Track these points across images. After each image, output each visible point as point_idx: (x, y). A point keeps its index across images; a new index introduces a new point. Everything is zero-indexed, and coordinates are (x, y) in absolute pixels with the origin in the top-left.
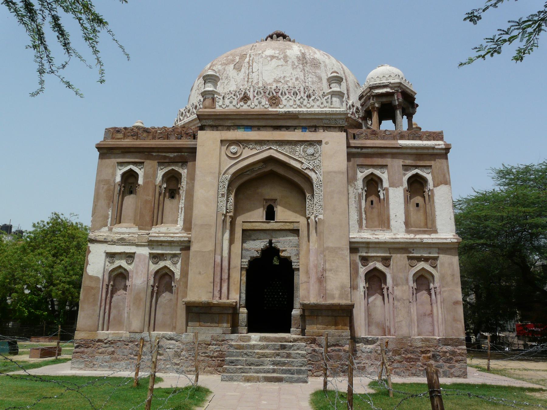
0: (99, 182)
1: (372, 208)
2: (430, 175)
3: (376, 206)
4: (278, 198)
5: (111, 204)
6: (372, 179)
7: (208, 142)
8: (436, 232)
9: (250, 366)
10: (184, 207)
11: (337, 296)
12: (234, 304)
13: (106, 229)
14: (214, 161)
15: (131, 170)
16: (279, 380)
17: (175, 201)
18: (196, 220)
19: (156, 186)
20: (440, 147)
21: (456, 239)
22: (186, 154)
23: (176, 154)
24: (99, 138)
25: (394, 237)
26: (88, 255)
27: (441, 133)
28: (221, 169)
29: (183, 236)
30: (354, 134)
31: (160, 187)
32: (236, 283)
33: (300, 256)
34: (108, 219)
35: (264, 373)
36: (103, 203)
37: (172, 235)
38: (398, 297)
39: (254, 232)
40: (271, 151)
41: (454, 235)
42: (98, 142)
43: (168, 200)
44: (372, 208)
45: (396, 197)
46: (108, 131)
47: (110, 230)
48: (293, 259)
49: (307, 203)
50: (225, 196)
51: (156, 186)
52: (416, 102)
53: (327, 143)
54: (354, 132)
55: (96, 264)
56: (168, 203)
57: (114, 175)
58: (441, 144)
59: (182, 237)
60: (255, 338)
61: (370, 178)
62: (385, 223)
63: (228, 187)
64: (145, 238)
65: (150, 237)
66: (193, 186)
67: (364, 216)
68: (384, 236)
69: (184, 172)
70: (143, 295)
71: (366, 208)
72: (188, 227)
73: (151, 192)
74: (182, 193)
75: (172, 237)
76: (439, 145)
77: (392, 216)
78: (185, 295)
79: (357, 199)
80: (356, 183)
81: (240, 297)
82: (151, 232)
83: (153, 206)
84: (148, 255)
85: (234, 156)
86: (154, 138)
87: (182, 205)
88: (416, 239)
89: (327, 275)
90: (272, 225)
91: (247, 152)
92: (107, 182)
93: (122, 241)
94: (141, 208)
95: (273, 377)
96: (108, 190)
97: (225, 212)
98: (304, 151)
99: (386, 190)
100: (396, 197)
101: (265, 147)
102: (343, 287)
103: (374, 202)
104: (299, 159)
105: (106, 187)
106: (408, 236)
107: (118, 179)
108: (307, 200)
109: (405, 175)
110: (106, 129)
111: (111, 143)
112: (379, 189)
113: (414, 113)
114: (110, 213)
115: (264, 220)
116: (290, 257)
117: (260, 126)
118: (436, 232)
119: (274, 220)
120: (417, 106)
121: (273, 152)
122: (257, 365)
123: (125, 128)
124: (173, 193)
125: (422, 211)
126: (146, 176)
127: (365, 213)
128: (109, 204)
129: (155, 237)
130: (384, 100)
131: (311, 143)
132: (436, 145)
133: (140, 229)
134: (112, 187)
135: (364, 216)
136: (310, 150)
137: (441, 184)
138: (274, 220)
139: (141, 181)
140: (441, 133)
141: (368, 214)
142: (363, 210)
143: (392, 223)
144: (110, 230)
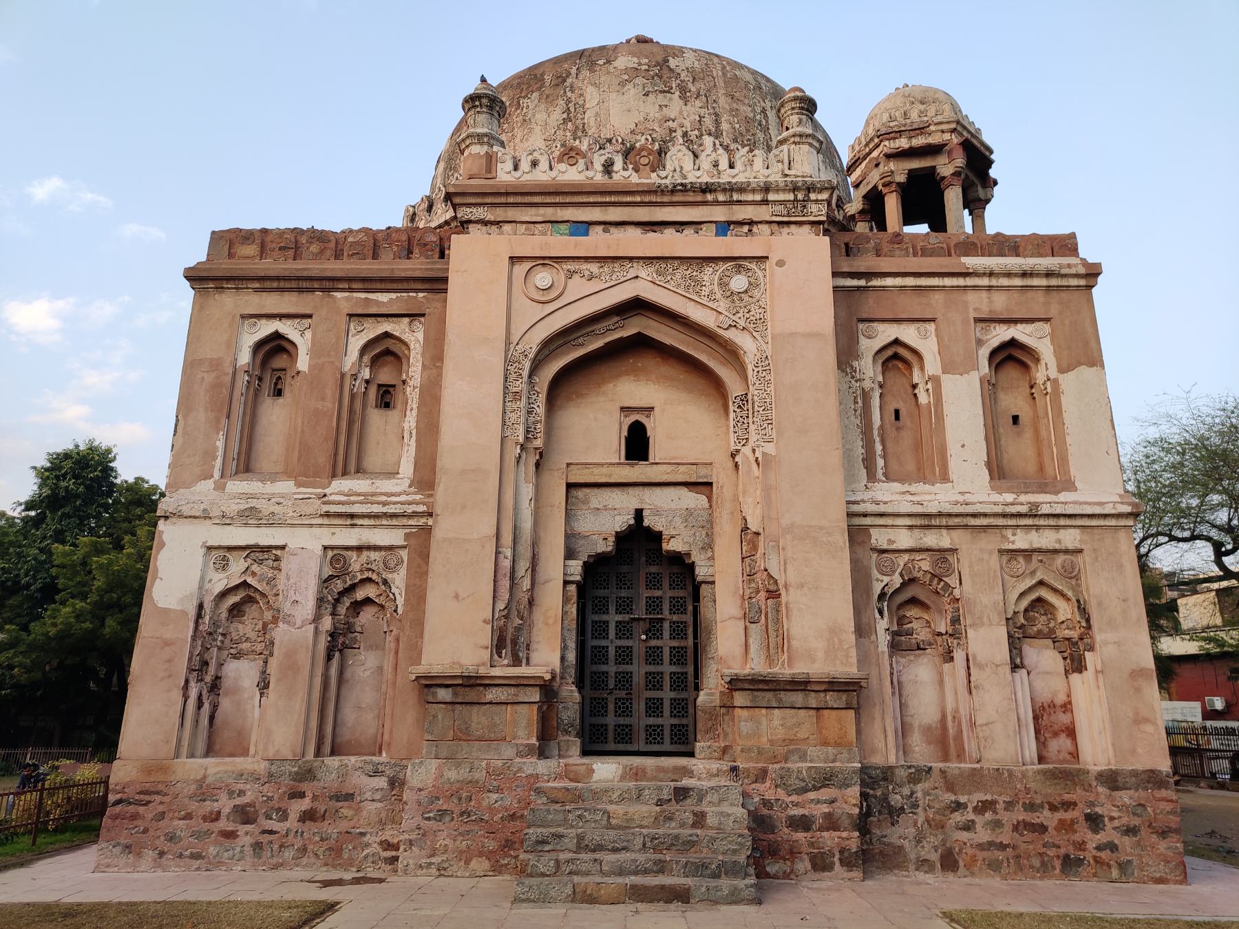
0: (191, 366)
1: (898, 429)
2: (1047, 341)
3: (909, 424)
4: (656, 404)
5: (224, 420)
6: (896, 356)
7: (476, 259)
8: (1070, 486)
9: (594, 851)
10: (417, 427)
11: (820, 655)
12: (548, 677)
13: (210, 484)
14: (495, 304)
15: (277, 336)
16: (680, 896)
17: (393, 415)
18: (449, 458)
19: (343, 376)
20: (1073, 271)
21: (1129, 504)
22: (421, 295)
23: (394, 296)
24: (198, 253)
25: (961, 498)
26: (158, 552)
27: (1073, 236)
28: (512, 332)
29: (414, 501)
30: (847, 245)
31: (355, 377)
32: (551, 622)
33: (716, 548)
34: (215, 458)
35: (636, 873)
36: (201, 416)
37: (384, 498)
38: (979, 658)
39: (596, 491)
40: (639, 282)
41: (1120, 496)
42: (192, 263)
43: (375, 411)
44: (898, 429)
45: (961, 404)
46: (217, 237)
47: (220, 487)
48: (698, 558)
49: (732, 415)
50: (524, 399)
51: (343, 376)
52: (993, 173)
53: (781, 263)
54: (847, 240)
55: (178, 574)
56: (376, 417)
57: (233, 345)
58: (1076, 265)
59: (410, 503)
60: (606, 770)
61: (890, 352)
62: (930, 464)
63: (530, 377)
64: (316, 506)
65: (325, 503)
66: (440, 375)
67: (879, 448)
68: (937, 497)
69: (414, 336)
70: (304, 659)
71: (882, 427)
72: (425, 480)
73: (330, 391)
74: (412, 395)
75: (384, 504)
76: (1069, 266)
77: (953, 448)
78: (417, 660)
79: (860, 404)
80: (855, 364)
81: (563, 659)
82: (327, 491)
83: (334, 424)
84: (319, 551)
85: (546, 297)
86: (338, 255)
87: (411, 421)
88: (1022, 504)
89: (791, 598)
90: (639, 472)
91: (578, 287)
92: (216, 364)
93: (249, 516)
94: (303, 431)
95: (663, 887)
96: (216, 386)
97: (521, 439)
98: (723, 284)
99: (936, 380)
100: (961, 404)
101: (620, 275)
102: (834, 631)
103: (903, 413)
104: (710, 304)
105: (210, 378)
106: (996, 497)
107: (245, 358)
108: (731, 408)
109: (980, 343)
110: (213, 233)
111: (226, 266)
112: (916, 380)
113: (988, 201)
114: (220, 444)
115: (623, 460)
116: (688, 555)
117: (610, 223)
118: (1070, 486)
119: (647, 459)
120: (995, 183)
121: (644, 285)
122: (615, 850)
123: (265, 231)
124: (386, 397)
125: (1028, 434)
126: (315, 351)
127: (883, 442)
128: (218, 420)
129: (339, 503)
130: (916, 164)
131: (737, 262)
132: (1061, 266)
133: (298, 485)
134: (228, 378)
135: (879, 448)
136: (739, 283)
137: (1080, 364)
138: (647, 459)
139: (303, 362)
140: (1073, 236)
141: (889, 445)
142: (876, 432)
143: (953, 464)
144: (220, 487)
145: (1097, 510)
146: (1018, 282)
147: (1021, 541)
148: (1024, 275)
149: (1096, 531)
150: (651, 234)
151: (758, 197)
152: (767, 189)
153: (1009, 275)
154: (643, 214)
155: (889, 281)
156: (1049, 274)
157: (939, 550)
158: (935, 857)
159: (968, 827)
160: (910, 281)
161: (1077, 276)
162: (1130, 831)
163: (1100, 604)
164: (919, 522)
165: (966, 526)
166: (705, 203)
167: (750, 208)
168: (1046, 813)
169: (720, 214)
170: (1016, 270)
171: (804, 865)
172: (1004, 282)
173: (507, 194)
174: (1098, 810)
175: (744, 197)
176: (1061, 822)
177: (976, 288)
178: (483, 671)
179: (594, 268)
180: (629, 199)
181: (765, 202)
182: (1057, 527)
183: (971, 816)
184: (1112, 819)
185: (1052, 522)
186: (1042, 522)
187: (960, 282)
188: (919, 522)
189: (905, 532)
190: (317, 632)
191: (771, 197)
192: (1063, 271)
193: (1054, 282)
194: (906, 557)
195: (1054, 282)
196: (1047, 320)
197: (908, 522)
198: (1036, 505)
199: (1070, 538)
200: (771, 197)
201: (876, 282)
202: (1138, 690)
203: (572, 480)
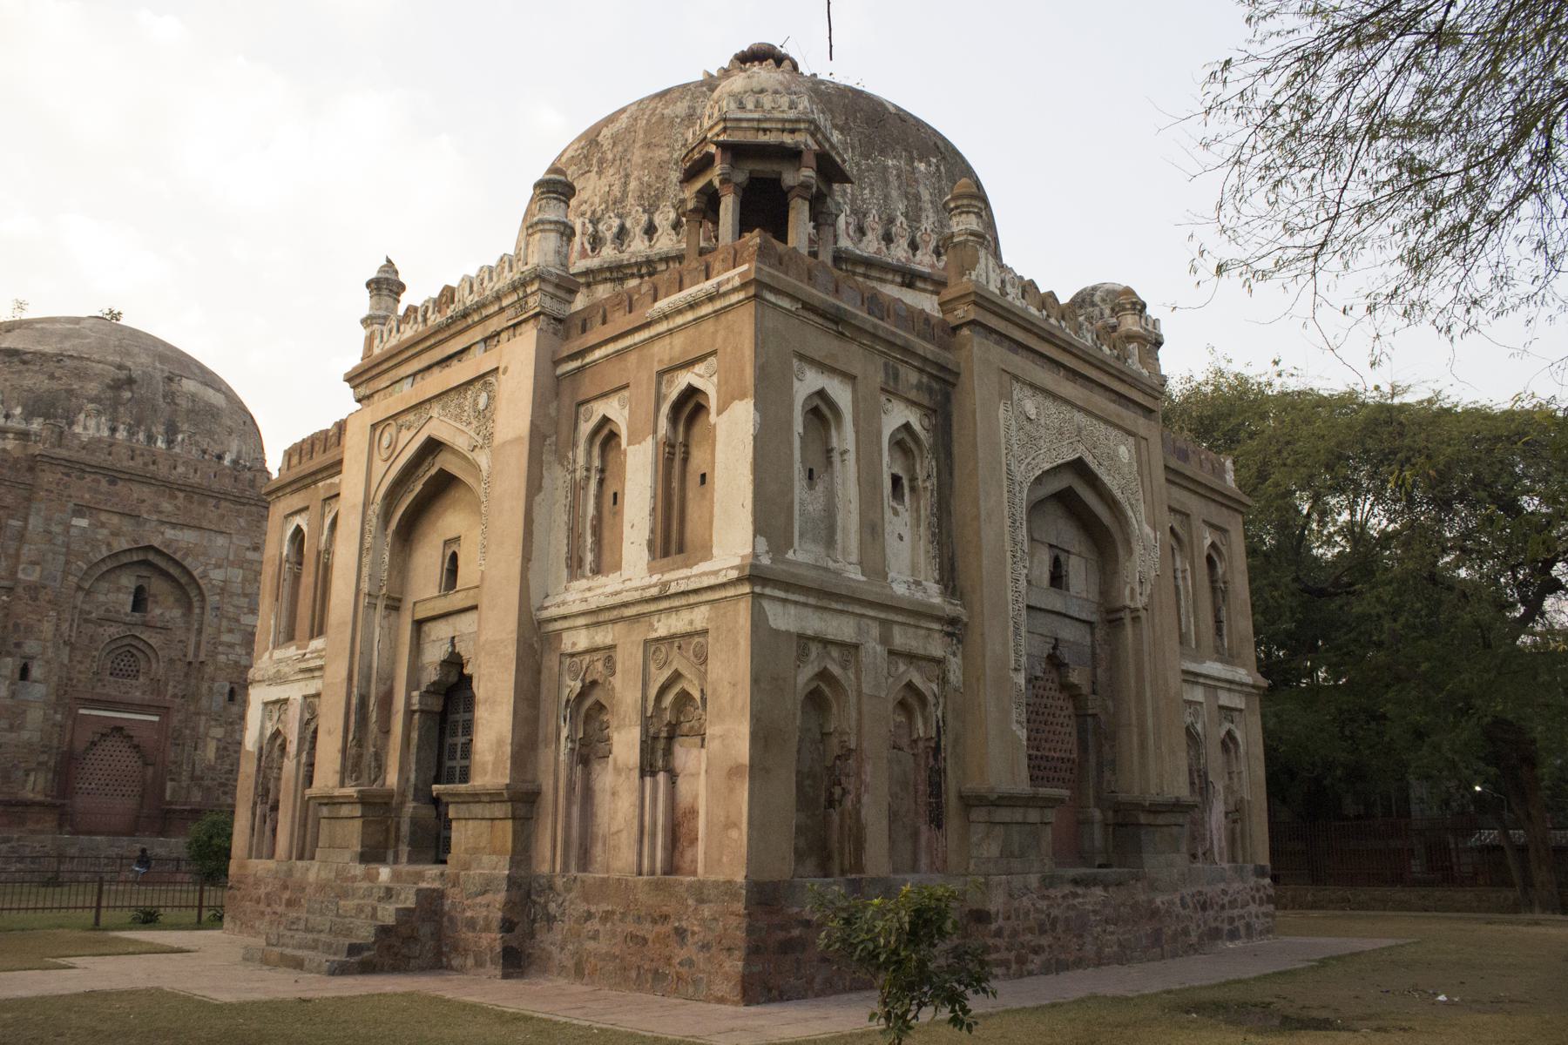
132: (719, 284)
137: (733, 399)
145: (712, 581)
146: (690, 316)
147: (663, 627)
148: (711, 298)
149: (723, 604)
150: (447, 371)
151: (496, 308)
152: (498, 298)
153: (679, 312)
154: (438, 354)
155: (598, 354)
156: (711, 298)
157: (604, 648)
158: (570, 964)
159: (595, 937)
160: (611, 348)
161: (735, 290)
162: (705, 947)
163: (715, 690)
164: (592, 619)
165: (622, 619)
166: (469, 327)
167: (495, 319)
168: (648, 925)
169: (477, 334)
170: (681, 305)
171: (470, 962)
172: (680, 320)
173: (401, 352)
174: (684, 924)
175: (485, 313)
176: (658, 934)
177: (659, 336)
178: (337, 793)
179: (411, 417)
180: (428, 343)
181: (502, 310)
182: (691, 606)
183: (597, 926)
184: (693, 933)
185: (683, 601)
186: (676, 602)
187: (645, 334)
188: (592, 619)
189: (584, 632)
190: (299, 763)
191: (505, 303)
192: (722, 290)
193: (719, 304)
194: (587, 658)
195: (719, 304)
196: (714, 353)
197: (581, 621)
198: (666, 584)
199: (699, 617)
200: (505, 303)
201: (588, 359)
202: (731, 790)
203: (419, 616)
